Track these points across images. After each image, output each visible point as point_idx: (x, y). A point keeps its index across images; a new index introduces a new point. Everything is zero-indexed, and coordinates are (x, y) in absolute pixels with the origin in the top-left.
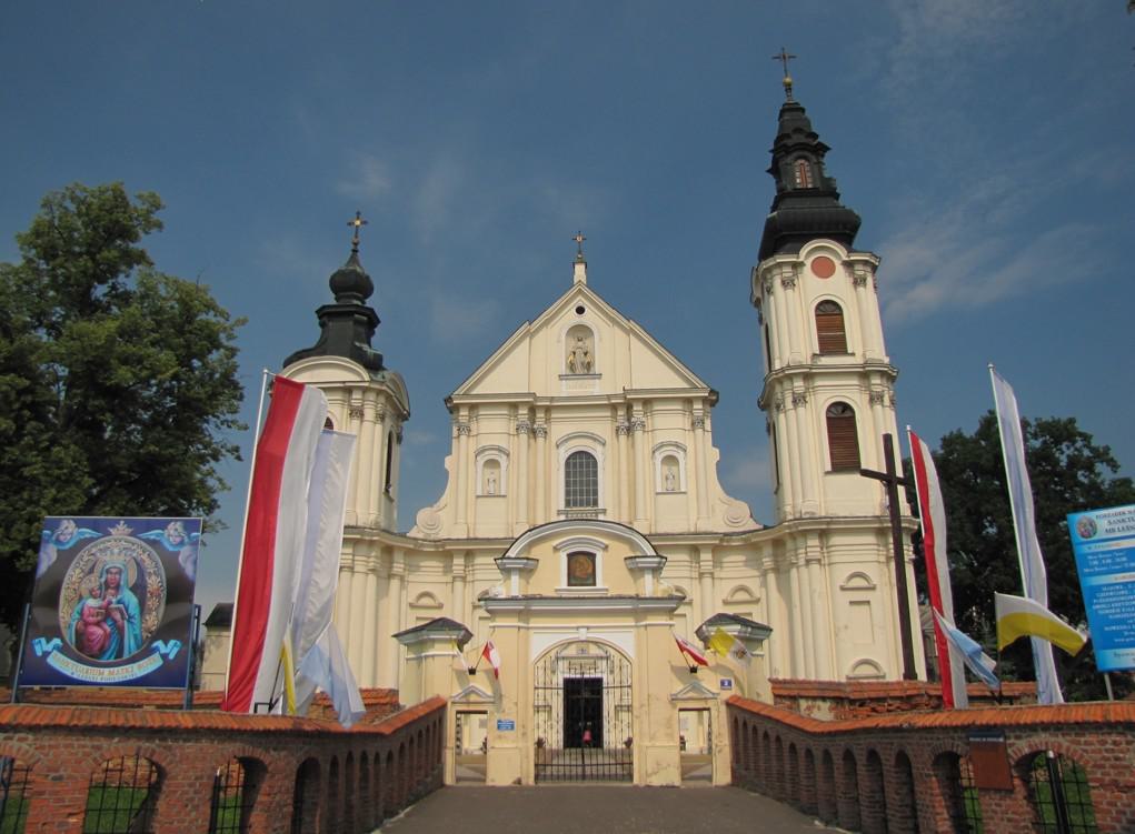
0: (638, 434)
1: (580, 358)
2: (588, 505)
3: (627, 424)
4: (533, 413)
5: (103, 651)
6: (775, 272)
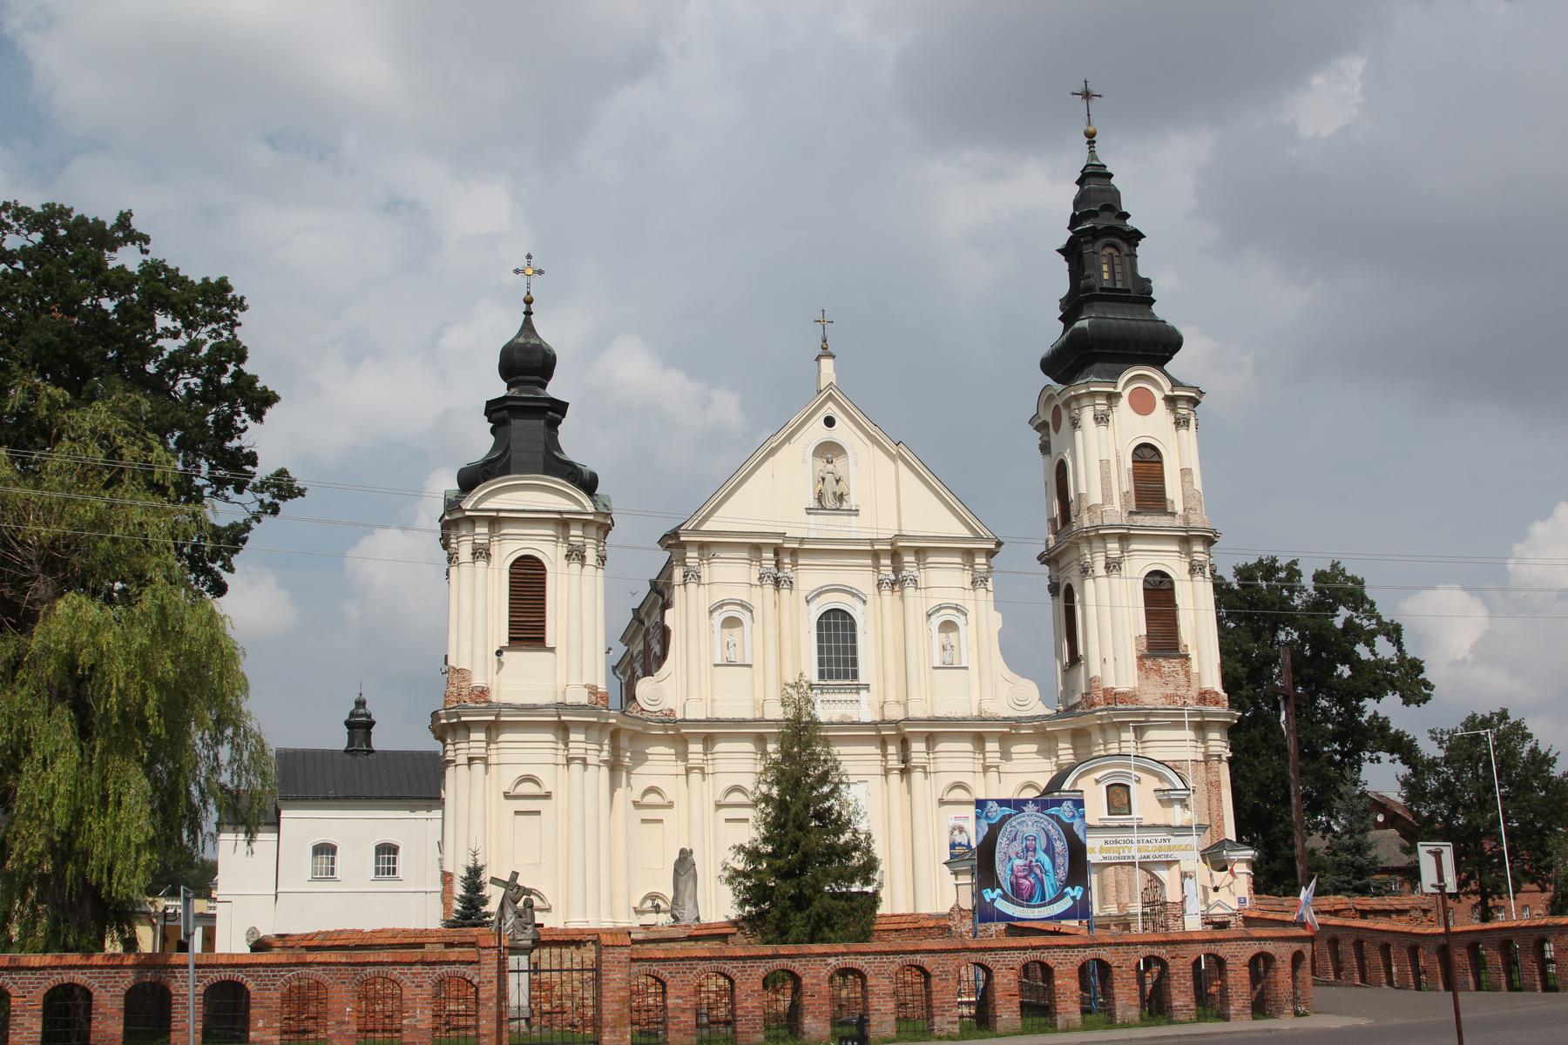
1: (830, 486)
2: (846, 677)
3: (893, 577)
4: (778, 556)
5: (1031, 896)
6: (1085, 401)
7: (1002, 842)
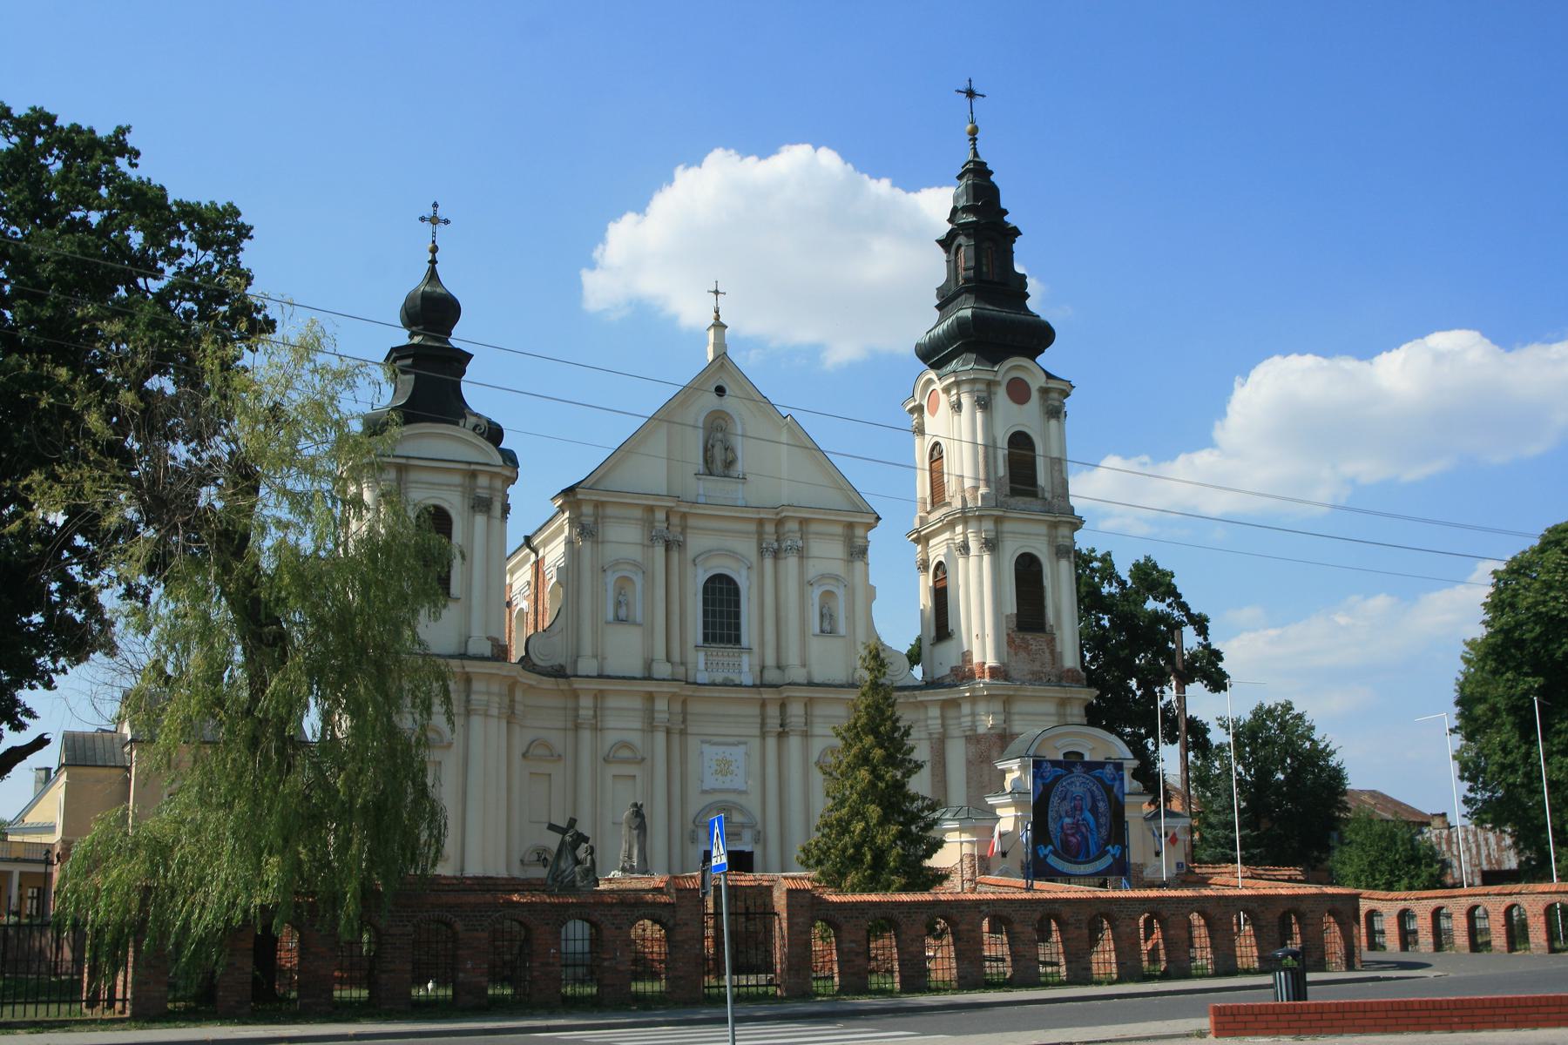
0: (791, 562)
3: (776, 545)
7: (1054, 800)
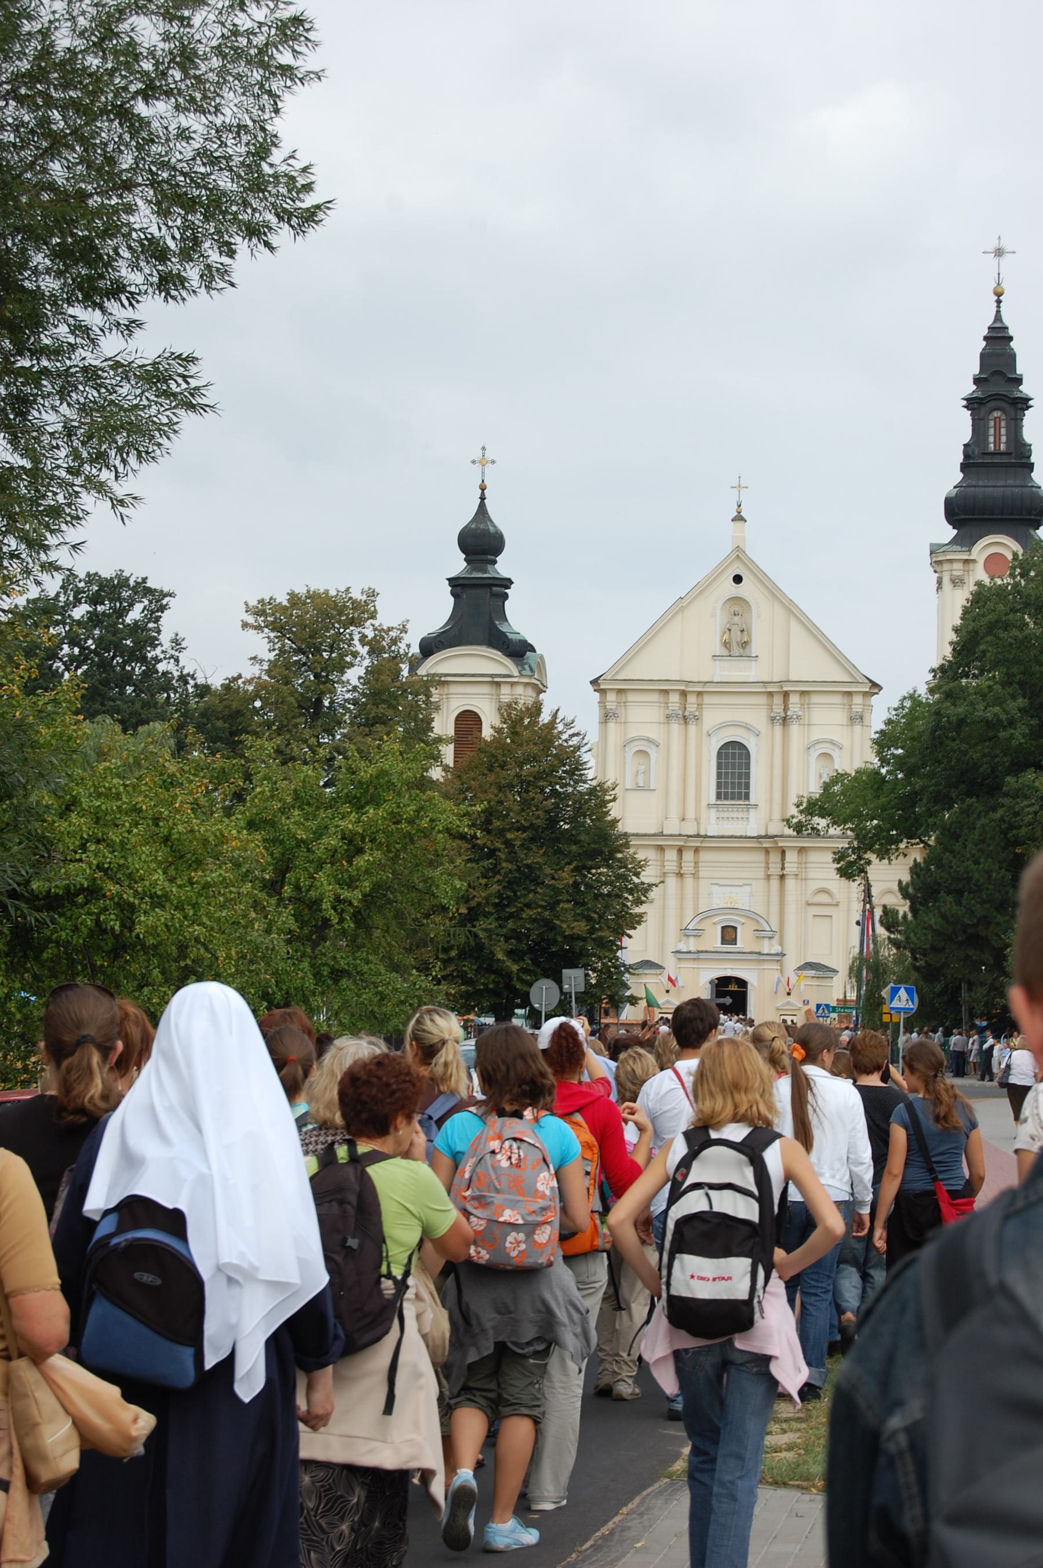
0: (794, 729)
2: (740, 799)
